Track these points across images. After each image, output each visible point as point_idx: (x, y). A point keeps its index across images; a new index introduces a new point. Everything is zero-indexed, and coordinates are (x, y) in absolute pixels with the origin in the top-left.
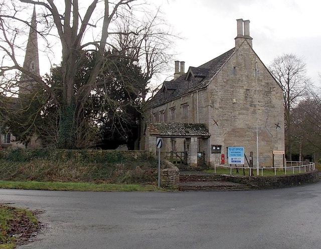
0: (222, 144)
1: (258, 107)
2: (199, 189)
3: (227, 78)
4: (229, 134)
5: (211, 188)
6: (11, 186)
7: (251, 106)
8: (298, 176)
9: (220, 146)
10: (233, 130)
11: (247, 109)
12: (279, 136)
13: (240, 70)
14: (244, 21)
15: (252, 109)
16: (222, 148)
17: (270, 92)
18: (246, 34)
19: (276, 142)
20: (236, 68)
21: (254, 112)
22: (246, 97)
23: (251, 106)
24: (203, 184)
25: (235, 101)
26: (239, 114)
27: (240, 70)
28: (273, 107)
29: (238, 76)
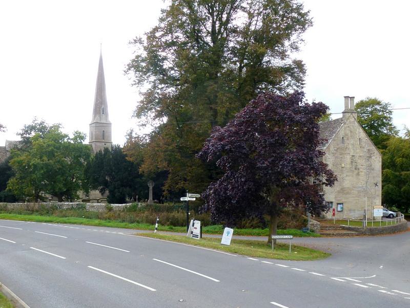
0: (333, 200)
1: (361, 170)
2: (108, 227)
3: (338, 147)
4: (339, 192)
5: (348, 235)
6: (93, 223)
7: (356, 169)
8: (395, 227)
9: (332, 203)
10: (342, 189)
11: (352, 171)
12: (377, 193)
13: (348, 139)
14: (350, 98)
15: (357, 171)
16: (334, 204)
17: (370, 157)
18: (347, 100)
19: (374, 198)
20: (344, 138)
21: (358, 174)
22: (352, 162)
23: (356, 169)
24: (331, 232)
25: (343, 165)
26: (347, 176)
27: (348, 139)
28: (373, 169)
29: (345, 145)
